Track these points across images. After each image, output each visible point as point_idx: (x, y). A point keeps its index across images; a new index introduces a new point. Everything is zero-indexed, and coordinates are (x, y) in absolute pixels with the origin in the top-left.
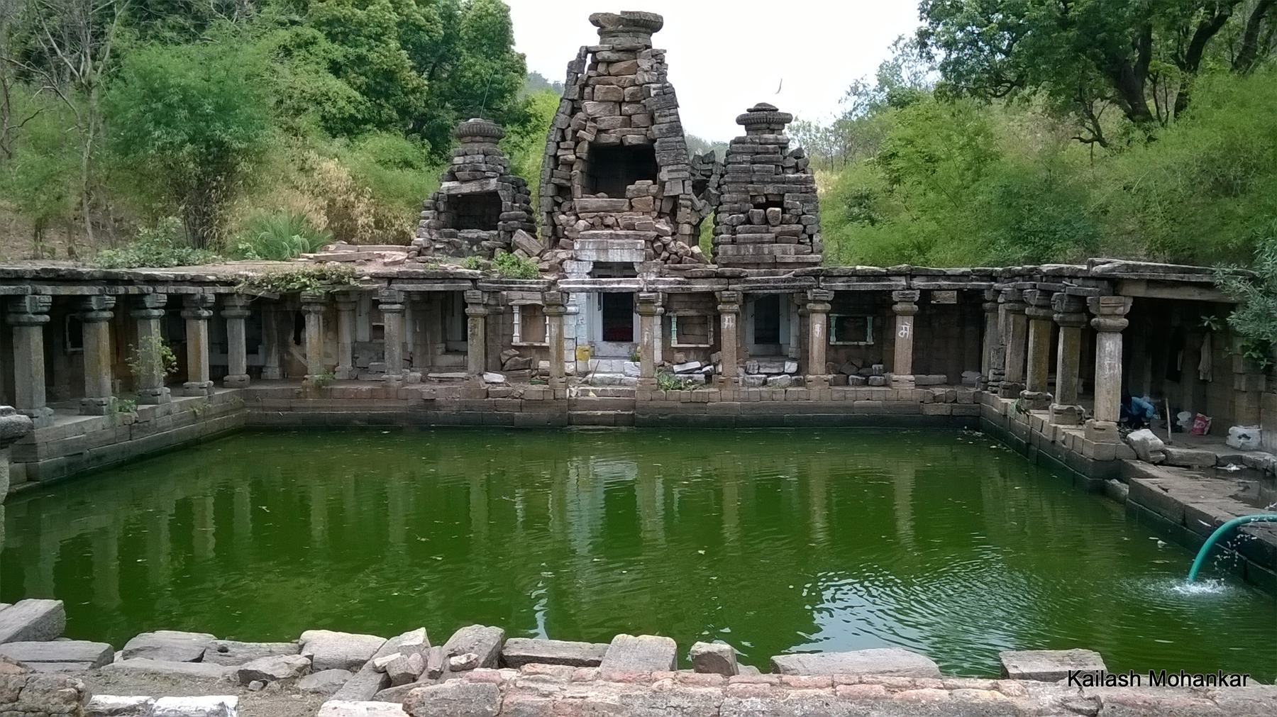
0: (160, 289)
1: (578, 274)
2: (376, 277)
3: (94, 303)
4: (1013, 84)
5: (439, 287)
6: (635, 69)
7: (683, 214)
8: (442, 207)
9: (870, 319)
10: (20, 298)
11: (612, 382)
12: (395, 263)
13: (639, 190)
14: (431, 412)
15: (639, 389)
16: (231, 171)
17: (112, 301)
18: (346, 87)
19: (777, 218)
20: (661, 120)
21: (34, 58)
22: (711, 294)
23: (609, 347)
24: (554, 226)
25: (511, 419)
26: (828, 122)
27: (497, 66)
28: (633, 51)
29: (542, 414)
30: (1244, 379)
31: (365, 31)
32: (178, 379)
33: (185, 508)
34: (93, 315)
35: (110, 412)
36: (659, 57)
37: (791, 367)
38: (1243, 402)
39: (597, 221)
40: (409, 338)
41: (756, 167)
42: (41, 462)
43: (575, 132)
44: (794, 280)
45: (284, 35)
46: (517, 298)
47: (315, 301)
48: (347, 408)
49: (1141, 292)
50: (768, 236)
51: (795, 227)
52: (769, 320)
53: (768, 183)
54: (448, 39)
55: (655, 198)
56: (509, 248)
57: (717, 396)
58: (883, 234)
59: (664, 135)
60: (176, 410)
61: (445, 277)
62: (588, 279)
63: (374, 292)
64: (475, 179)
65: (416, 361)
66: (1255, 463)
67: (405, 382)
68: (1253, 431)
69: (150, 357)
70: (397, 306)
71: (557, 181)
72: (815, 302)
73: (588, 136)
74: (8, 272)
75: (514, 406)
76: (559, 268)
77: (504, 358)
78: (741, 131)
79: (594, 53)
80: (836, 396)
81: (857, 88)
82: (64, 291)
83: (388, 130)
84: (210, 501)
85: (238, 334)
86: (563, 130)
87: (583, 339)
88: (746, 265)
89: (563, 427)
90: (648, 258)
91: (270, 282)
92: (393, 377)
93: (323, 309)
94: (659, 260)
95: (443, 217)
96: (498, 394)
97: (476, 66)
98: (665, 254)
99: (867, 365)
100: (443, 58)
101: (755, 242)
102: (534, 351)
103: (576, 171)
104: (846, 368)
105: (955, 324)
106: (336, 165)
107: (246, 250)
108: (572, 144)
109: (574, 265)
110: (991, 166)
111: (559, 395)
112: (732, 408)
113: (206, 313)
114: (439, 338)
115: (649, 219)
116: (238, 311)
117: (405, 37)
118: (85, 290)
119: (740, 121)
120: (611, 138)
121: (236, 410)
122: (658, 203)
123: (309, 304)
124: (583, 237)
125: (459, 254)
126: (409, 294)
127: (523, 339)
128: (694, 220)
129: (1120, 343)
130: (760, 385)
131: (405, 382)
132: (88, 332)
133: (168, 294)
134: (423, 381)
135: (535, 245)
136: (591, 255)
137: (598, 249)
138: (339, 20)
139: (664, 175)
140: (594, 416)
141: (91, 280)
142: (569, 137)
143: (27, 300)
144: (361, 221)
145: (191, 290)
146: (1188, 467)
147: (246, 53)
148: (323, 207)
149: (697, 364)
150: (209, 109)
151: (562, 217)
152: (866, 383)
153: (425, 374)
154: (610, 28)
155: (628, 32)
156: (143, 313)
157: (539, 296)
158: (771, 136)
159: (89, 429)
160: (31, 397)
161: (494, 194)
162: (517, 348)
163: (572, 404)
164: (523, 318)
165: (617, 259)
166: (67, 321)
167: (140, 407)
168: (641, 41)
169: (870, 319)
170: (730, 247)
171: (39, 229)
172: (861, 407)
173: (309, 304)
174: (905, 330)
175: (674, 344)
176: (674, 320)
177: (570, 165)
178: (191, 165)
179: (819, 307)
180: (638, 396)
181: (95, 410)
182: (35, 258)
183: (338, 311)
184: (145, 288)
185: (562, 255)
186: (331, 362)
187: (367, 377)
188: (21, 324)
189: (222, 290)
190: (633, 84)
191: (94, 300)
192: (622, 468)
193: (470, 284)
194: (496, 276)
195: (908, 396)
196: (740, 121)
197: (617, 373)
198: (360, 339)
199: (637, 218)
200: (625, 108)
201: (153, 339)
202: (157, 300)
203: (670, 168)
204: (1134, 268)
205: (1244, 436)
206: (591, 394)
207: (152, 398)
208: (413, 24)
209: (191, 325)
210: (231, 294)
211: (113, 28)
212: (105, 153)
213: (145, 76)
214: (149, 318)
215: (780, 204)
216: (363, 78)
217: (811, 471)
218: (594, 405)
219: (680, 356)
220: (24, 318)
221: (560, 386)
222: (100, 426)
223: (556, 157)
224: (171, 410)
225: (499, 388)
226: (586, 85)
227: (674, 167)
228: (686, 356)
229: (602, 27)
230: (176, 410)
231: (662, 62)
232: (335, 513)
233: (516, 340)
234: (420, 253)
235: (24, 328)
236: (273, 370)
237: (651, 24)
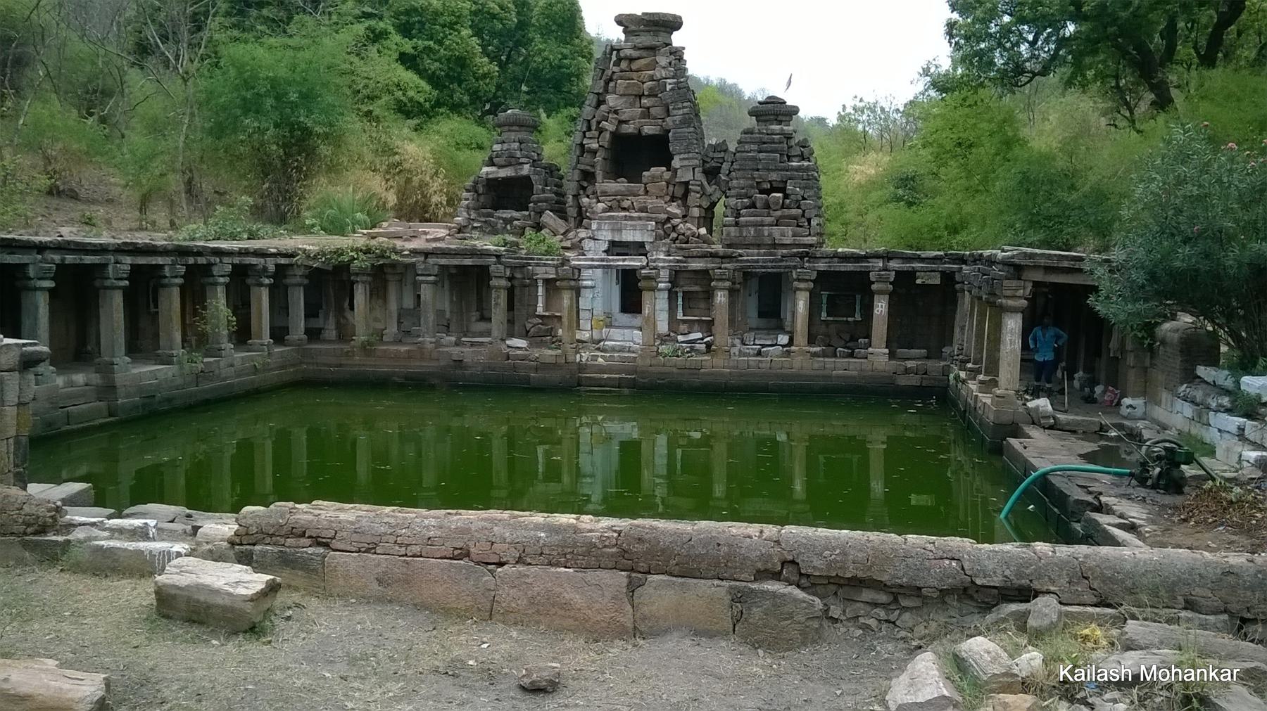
0: (226, 260)
1: (595, 250)
2: (414, 252)
3: (167, 271)
4: (1035, 74)
5: (468, 262)
6: (654, 65)
7: (693, 198)
8: (481, 190)
9: (858, 297)
10: (104, 266)
11: (622, 350)
12: (436, 240)
13: (653, 177)
14: (459, 372)
15: (641, 356)
16: (311, 154)
17: (182, 270)
18: (415, 78)
19: (777, 203)
20: (675, 112)
21: (143, 49)
22: (705, 272)
23: (625, 318)
24: (580, 208)
25: (527, 380)
26: (900, 103)
27: (565, 51)
28: (652, 49)
29: (555, 376)
30: (1132, 355)
31: (441, 20)
32: (242, 335)
33: (246, 448)
34: (166, 281)
35: (179, 363)
36: (678, 54)
37: (783, 339)
38: (1132, 376)
39: (615, 204)
40: (447, 306)
41: (762, 155)
42: (120, 401)
43: (599, 123)
44: (781, 261)
45: (360, 28)
46: (542, 273)
47: (362, 272)
48: (388, 366)
49: (1039, 276)
50: (768, 220)
51: (794, 211)
52: (766, 295)
54: (522, 25)
55: (668, 183)
56: (538, 227)
57: (709, 364)
58: (923, 216)
59: (677, 127)
60: (238, 363)
61: (473, 253)
62: (604, 256)
63: (413, 265)
64: (510, 165)
65: (452, 328)
66: (1132, 429)
67: (438, 344)
68: (1138, 402)
69: (218, 318)
70: (432, 278)
71: (583, 167)
72: (799, 280)
73: (610, 126)
74: (95, 245)
75: (530, 368)
76: (577, 247)
77: (528, 326)
78: (616, 34)
79: (618, 51)
80: (816, 366)
81: (929, 68)
82: (141, 260)
83: (460, 114)
84: (269, 444)
85: (298, 300)
86: (589, 121)
87: (599, 310)
88: (747, 246)
89: (573, 388)
90: (658, 238)
91: (324, 255)
92: (428, 340)
93: (369, 279)
94: (668, 241)
95: (482, 199)
96: (517, 357)
97: (545, 50)
98: (674, 235)
99: (854, 339)
100: (518, 44)
101: (756, 225)
103: (599, 158)
104: (835, 341)
105: (927, 305)
106: (416, 149)
107: (313, 226)
108: (596, 133)
109: (592, 243)
110: (1017, 150)
111: (570, 359)
112: (722, 374)
113: (267, 281)
114: (474, 307)
115: (661, 203)
116: (298, 280)
117: (481, 25)
118: (160, 260)
119: (620, 20)
120: (629, 129)
121: (293, 365)
122: (671, 188)
123: (357, 274)
124: (601, 218)
125: (494, 232)
126: (443, 268)
127: (546, 308)
128: (705, 204)
129: (1020, 322)
131: (441, 346)
132: (163, 293)
133: (233, 265)
134: (457, 344)
135: (561, 225)
136: (606, 235)
137: (613, 230)
138: (415, 10)
139: (676, 163)
141: (164, 252)
142: (594, 127)
143: (110, 268)
144: (435, 199)
145: (254, 261)
146: (1074, 432)
147: (326, 46)
148: (396, 186)
149: (699, 335)
150: (293, 97)
151: (585, 200)
152: (851, 355)
153: (459, 338)
154: (633, 28)
156: (211, 280)
157: (553, 270)
158: (778, 127)
159: (161, 376)
160: (113, 347)
161: (527, 178)
162: (539, 316)
163: (582, 367)
164: (547, 291)
165: (630, 239)
166: (144, 285)
167: (206, 360)
168: (662, 38)
169: (858, 297)
170: (733, 229)
171: (144, 203)
172: (838, 377)
173: (357, 274)
174: (881, 307)
175: (680, 316)
176: (680, 295)
177: (594, 152)
178: (274, 147)
179: (802, 285)
180: (640, 362)
181: (168, 360)
182: (141, 229)
183: (386, 281)
184: (212, 259)
185: (582, 233)
186: (380, 326)
187: (409, 340)
188: (107, 288)
189: (283, 261)
190: (652, 79)
191: (167, 268)
192: (628, 429)
193: (494, 259)
194: (524, 252)
195: (880, 368)
196: (620, 20)
197: (627, 338)
198: (405, 306)
199: (651, 202)
200: (644, 101)
201: (219, 304)
202: (223, 268)
204: (1032, 256)
205: (1131, 406)
206: (600, 360)
207: (217, 352)
208: (488, 13)
209: (254, 290)
210: (292, 265)
211: (213, 23)
212: (199, 135)
213: (240, 69)
214: (216, 284)
215: (782, 190)
216: (437, 64)
217: (792, 433)
218: (601, 369)
219: (683, 328)
220: (108, 283)
221: (571, 352)
222: (170, 374)
223: (582, 145)
224: (233, 363)
225: (519, 352)
226: (611, 80)
228: (689, 327)
229: (626, 27)
230: (238, 363)
231: (680, 59)
232: (380, 456)
233: (540, 310)
234: (459, 231)
235: (108, 291)
236: (330, 333)
237: (673, 24)
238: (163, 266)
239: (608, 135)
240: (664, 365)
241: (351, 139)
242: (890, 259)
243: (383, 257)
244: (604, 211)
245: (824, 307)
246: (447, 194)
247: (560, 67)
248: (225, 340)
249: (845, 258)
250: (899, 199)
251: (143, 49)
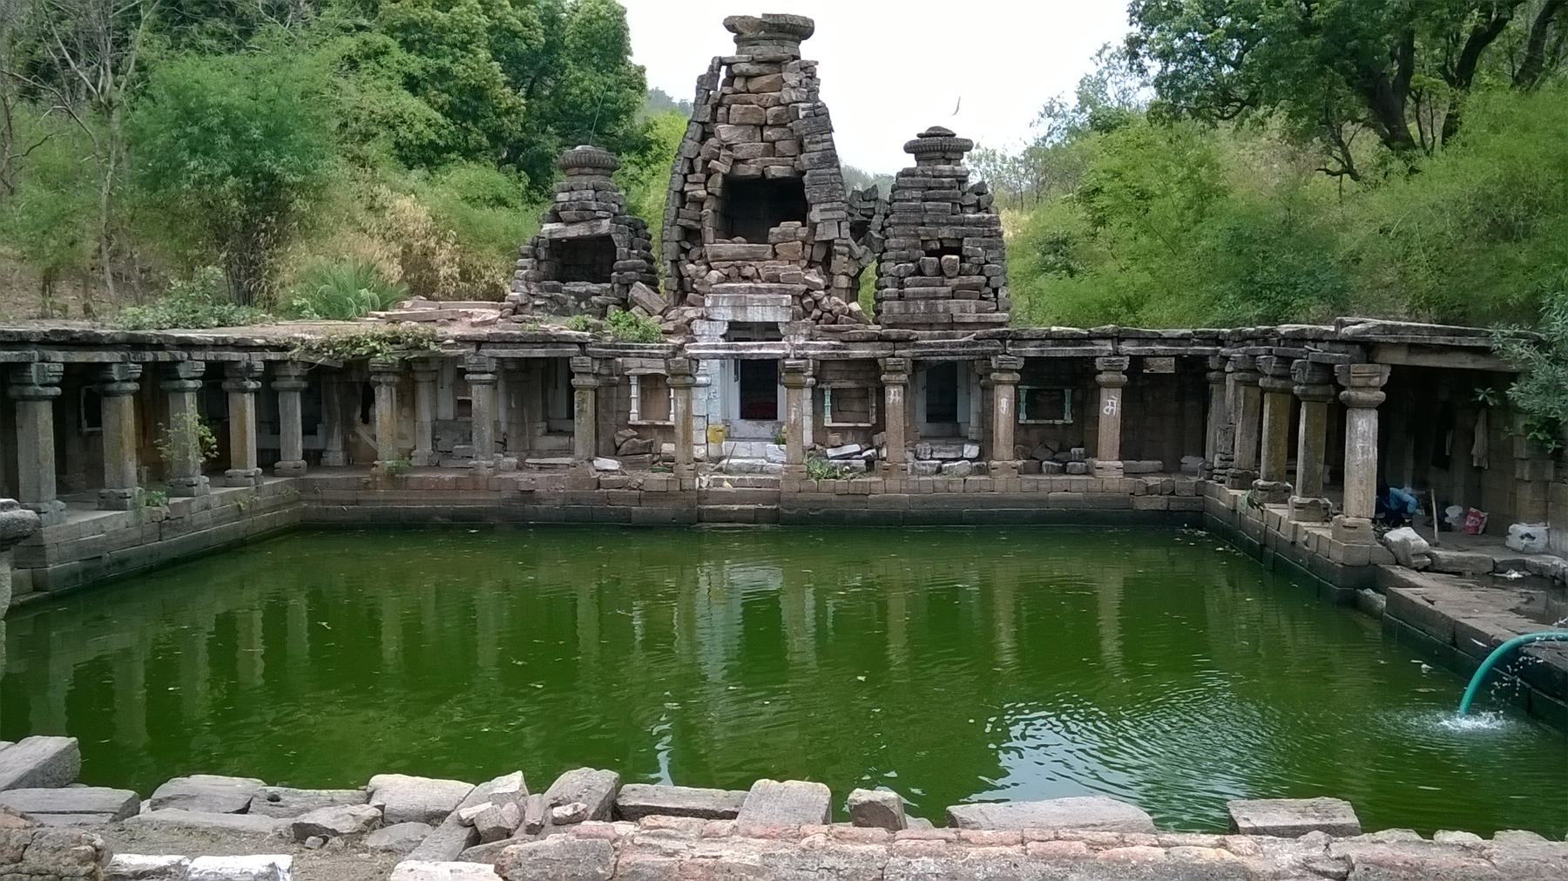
0: (197, 355)
1: (709, 337)
2: (462, 341)
3: (115, 373)
4: (1244, 104)
5: (539, 353)
6: (779, 85)
7: (839, 263)
8: (543, 255)
9: (1068, 392)
10: (24, 366)
11: (751, 470)
13: (784, 234)
14: (528, 507)
15: (785, 478)
16: (283, 210)
17: (137, 370)
18: (425, 107)
20: (811, 147)
21: (42, 72)
22: (872, 362)
23: (748, 427)
24: (681, 277)
25: (627, 515)
26: (1016, 151)
28: (777, 63)
29: (666, 509)
30: (1527, 465)
31: (448, 38)
32: (218, 466)
33: (227, 625)
34: (114, 387)
35: (135, 506)
36: (809, 70)
37: (971, 451)
38: (1526, 494)
39: (733, 271)
40: (502, 415)
41: (929, 205)
42: (51, 567)
43: (706, 162)
44: (975, 345)
45: (349, 44)
46: (635, 366)
47: (387, 370)
48: (426, 502)
49: (1401, 358)
51: (976, 279)
52: (944, 393)
53: (944, 225)
54: (551, 48)
55: (804, 243)
56: (625, 305)
57: (880, 487)
58: (1085, 288)
59: (815, 166)
60: (216, 504)
61: (547, 340)
62: (722, 343)
63: (459, 358)
64: (583, 220)
65: (511, 444)
66: (1541, 568)
67: (497, 469)
68: (1538, 530)
70: (488, 377)
71: (684, 222)
72: (1001, 370)
73: (722, 167)
74: (10, 335)
75: (631, 498)
76: (686, 329)
77: (619, 440)
79: (729, 65)
80: (1026, 486)
81: (1052, 108)
82: (79, 357)
83: (476, 160)
84: (258, 615)
85: (293, 411)
86: (691, 160)
87: (716, 416)
88: (916, 326)
89: (691, 525)
90: (796, 317)
91: (331, 346)
92: (483, 464)
93: (397, 379)
94: (809, 320)
95: (544, 267)
96: (611, 484)
97: (585, 81)
98: (816, 312)
99: (1064, 448)
100: (544, 72)
101: (926, 298)
102: (655, 431)
103: (708, 210)
104: (1039, 452)
105: (1173, 398)
106: (413, 203)
107: (302, 307)
108: (702, 177)
109: (705, 325)
110: (1217, 204)
111: (686, 485)
112: (899, 501)
113: (253, 385)
114: (539, 415)
115: (797, 269)
116: (293, 382)
117: (498, 46)
118: (105, 357)
120: (751, 170)
121: (289, 504)
122: (808, 249)
123: (379, 373)
124: (716, 291)
125: (564, 312)
126: (502, 361)
127: (642, 416)
128: (853, 271)
129: (1376, 422)
130: (933, 473)
131: (498, 469)
132: (108, 407)
133: (206, 362)
134: (519, 468)
135: (657, 301)
136: (725, 314)
137: (734, 306)
138: (416, 24)
139: (815, 215)
140: (730, 511)
141: (112, 344)
142: (699, 168)
143: (33, 368)
144: (443, 271)
145: (234, 356)
146: (1459, 574)
147: (302, 65)
148: (396, 254)
149: (856, 448)
150: (256, 134)
152: (1063, 471)
153: (522, 460)
154: (749, 34)
155: (771, 39)
156: (176, 384)
157: (662, 363)
158: (947, 167)
159: (109, 527)
162: (635, 427)
163: (702, 496)
164: (643, 391)
165: (758, 318)
166: (83, 394)
167: (172, 501)
168: (787, 51)
169: (1068, 392)
170: (896, 303)
171: (49, 281)
172: (1057, 501)
173: (379, 373)
174: (1111, 405)
175: (828, 423)
176: (828, 394)
177: (700, 203)
178: (235, 203)
179: (1005, 377)
180: (784, 487)
181: (117, 503)
182: (43, 316)
183: (415, 382)
184: (178, 354)
185: (691, 313)
186: (407, 445)
187: (451, 463)
189: (273, 356)
190: (778, 103)
191: (115, 368)
192: (764, 575)
193: (577, 349)
194: (609, 339)
195: (1115, 487)
197: (757, 458)
198: (442, 416)
199: (783, 268)
200: (767, 133)
201: (188, 417)
202: (192, 368)
203: (823, 206)
204: (1392, 330)
205: (1528, 535)
206: (726, 484)
207: (187, 489)
208: (508, 29)
209: (234, 399)
211: (139, 34)
213: (178, 94)
214: (183, 390)
215: (957, 251)
216: (446, 96)
217: (996, 578)
218: (729, 498)
219: (834, 438)
220: (30, 391)
221: (687, 474)
222: (122, 523)
223: (682, 193)
224: (210, 504)
225: (613, 477)
226: (720, 104)
227: (828, 206)
228: (843, 438)
229: (739, 33)
230: (216, 504)
231: (812, 77)
232: (412, 631)
233: (634, 418)
234: (515, 311)
235: (30, 404)
236: (335, 454)
237: (799, 30)
238: (110, 364)
241: (336, 192)
243: (418, 348)
244: (720, 281)
246: (460, 266)
247: (605, 101)
248: (199, 471)
250: (1049, 268)
251: (42, 72)
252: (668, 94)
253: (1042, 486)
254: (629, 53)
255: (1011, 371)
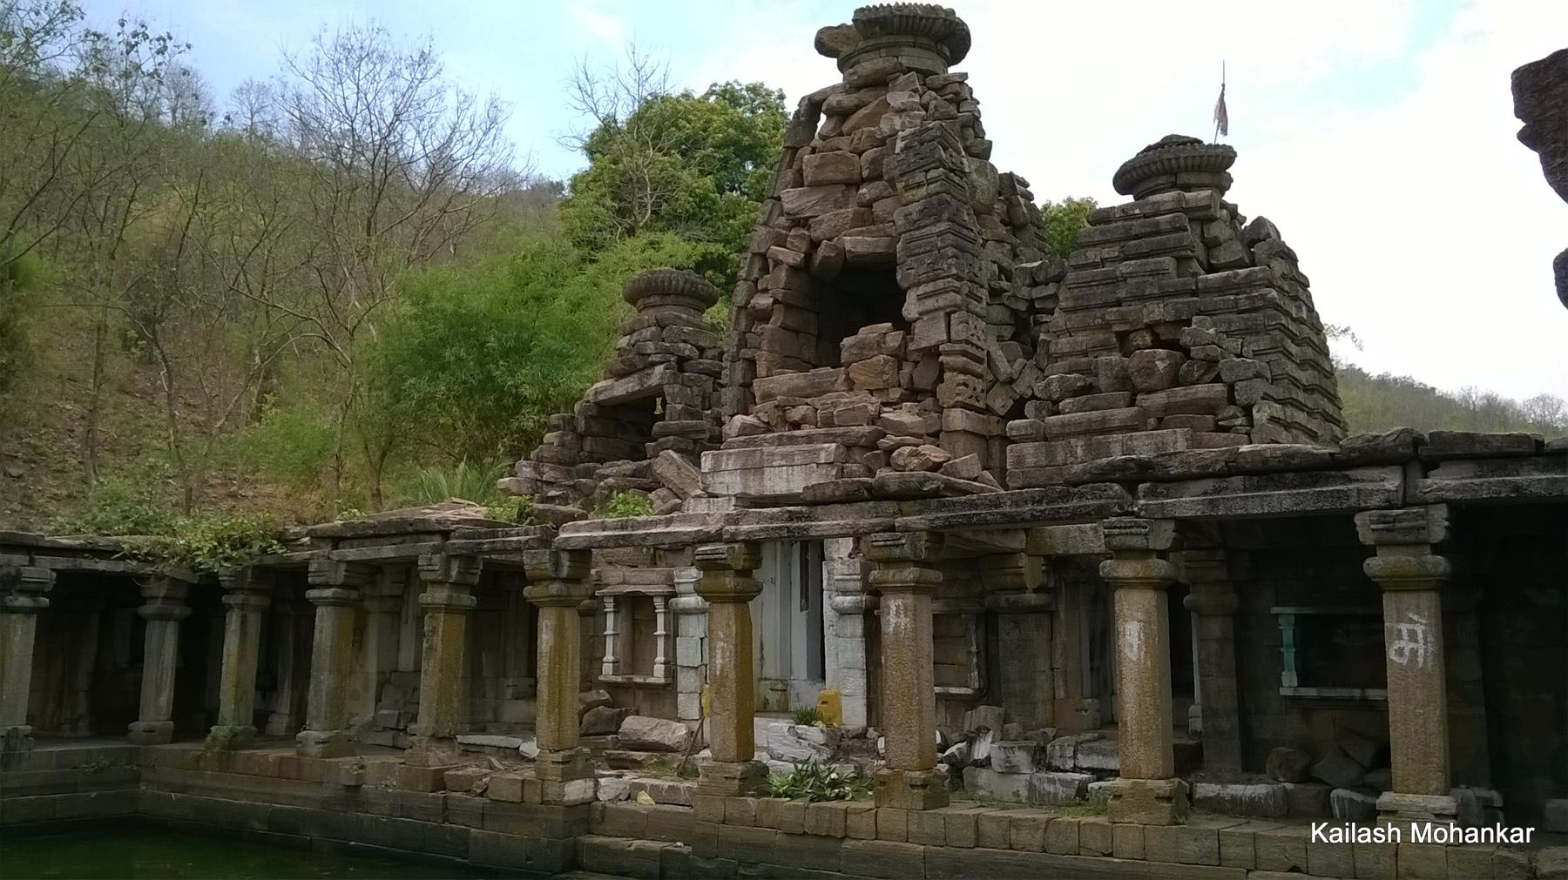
13: (861, 346)
20: (909, 195)
51: (1202, 390)
53: (1151, 297)
78: (826, 74)
80: (1191, 848)
101: (1087, 431)
102: (640, 694)
111: (552, 791)
119: (827, 43)
130: (1068, 804)
137: (745, 470)
139: (910, 309)
140: (622, 852)
155: (877, 48)
196: (827, 43)
203: (922, 290)
206: (644, 798)
218: (641, 826)
227: (930, 287)
239: (783, 274)
240: (756, 822)
242: (1429, 466)
245: (1289, 656)
249: (1265, 473)
252: (1365, 371)
253: (1230, 851)
254: (1511, 404)
255: (1144, 553)
